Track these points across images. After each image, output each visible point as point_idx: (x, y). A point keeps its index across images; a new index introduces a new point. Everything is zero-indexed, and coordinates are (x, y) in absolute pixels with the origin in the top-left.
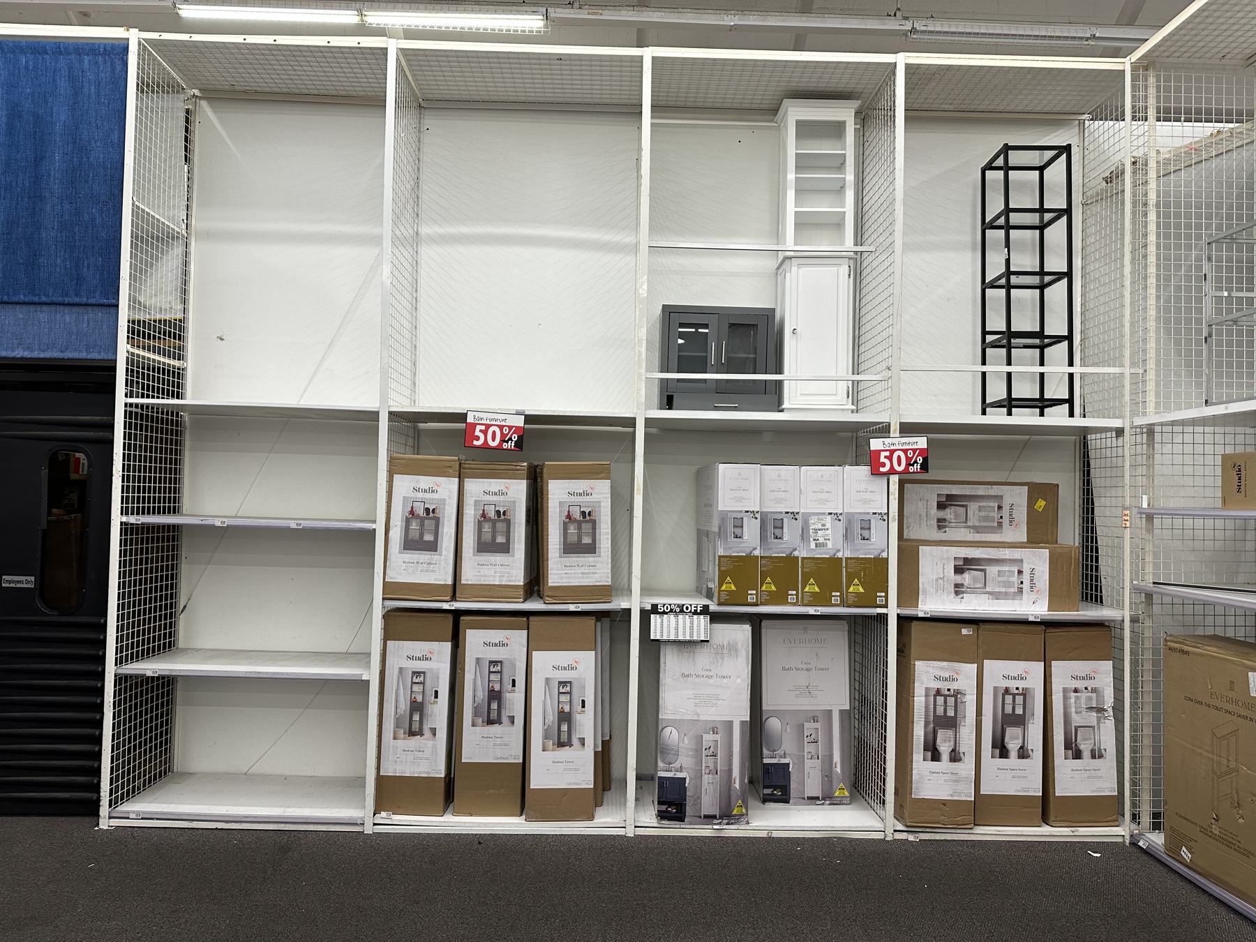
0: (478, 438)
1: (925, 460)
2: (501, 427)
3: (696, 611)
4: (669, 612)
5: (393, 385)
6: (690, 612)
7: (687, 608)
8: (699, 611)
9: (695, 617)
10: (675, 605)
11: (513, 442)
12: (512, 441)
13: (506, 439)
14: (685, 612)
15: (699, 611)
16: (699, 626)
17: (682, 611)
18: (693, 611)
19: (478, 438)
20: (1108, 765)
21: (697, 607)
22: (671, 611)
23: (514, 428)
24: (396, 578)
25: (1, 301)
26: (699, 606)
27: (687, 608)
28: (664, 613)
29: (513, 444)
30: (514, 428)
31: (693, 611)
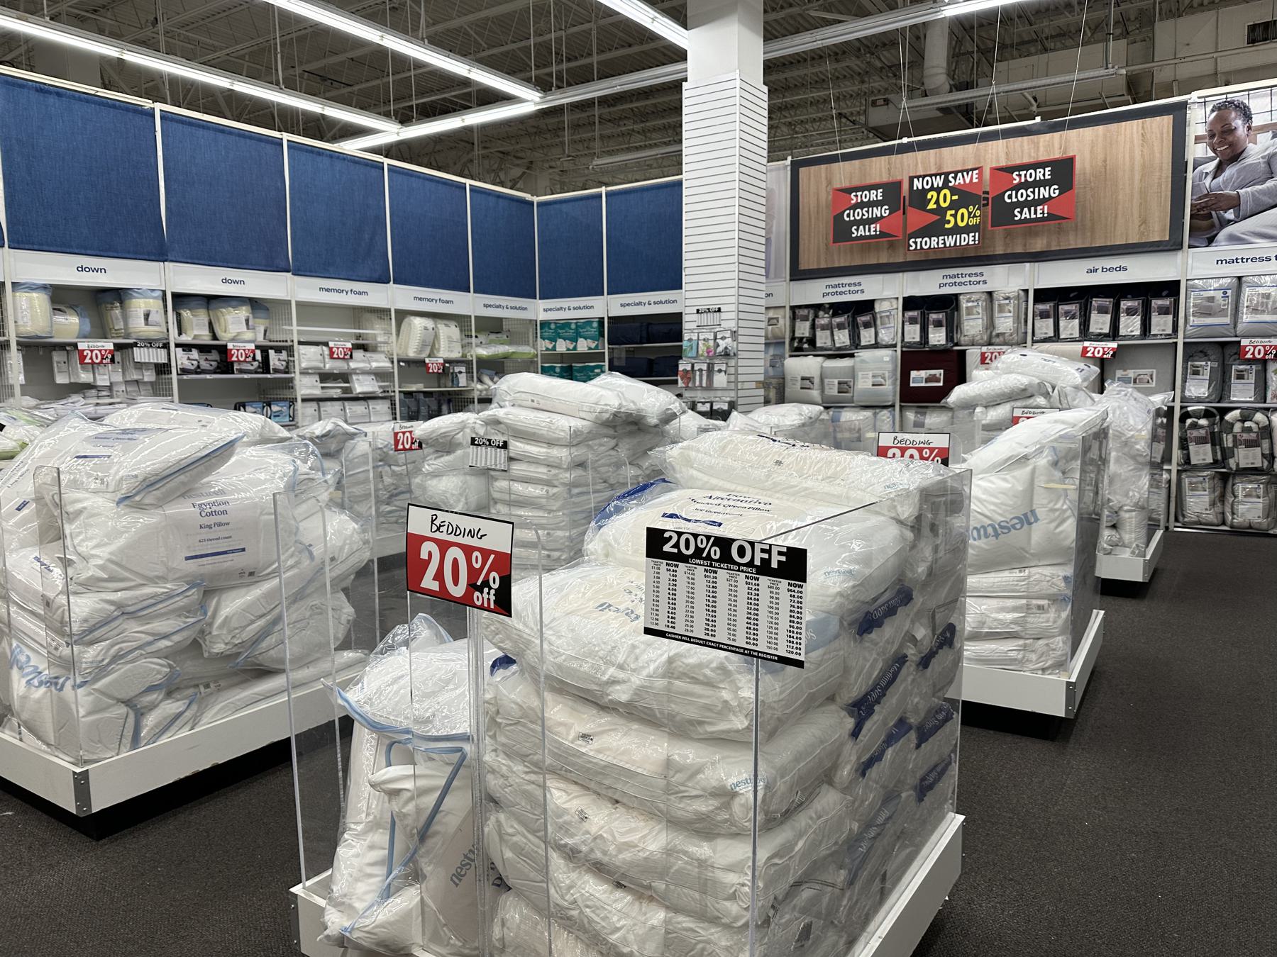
0: (949, 222)
1: (113, 356)
2: (100, 351)
3: (765, 562)
4: (692, 556)
5: (763, 201)
6: (751, 564)
7: (741, 551)
8: (774, 565)
9: (764, 581)
10: (708, 538)
11: (493, 592)
12: (490, 588)
13: (479, 583)
14: (735, 563)
15: (774, 565)
16: (774, 609)
17: (726, 558)
18: (757, 562)
19: (949, 222)
20: (931, 319)
21: (769, 551)
22: (698, 553)
23: (492, 557)
24: (268, 448)
25: (1275, 90)
26: (774, 552)
27: (741, 551)
28: (681, 558)
29: (493, 598)
30: (492, 557)
31: (757, 562)
